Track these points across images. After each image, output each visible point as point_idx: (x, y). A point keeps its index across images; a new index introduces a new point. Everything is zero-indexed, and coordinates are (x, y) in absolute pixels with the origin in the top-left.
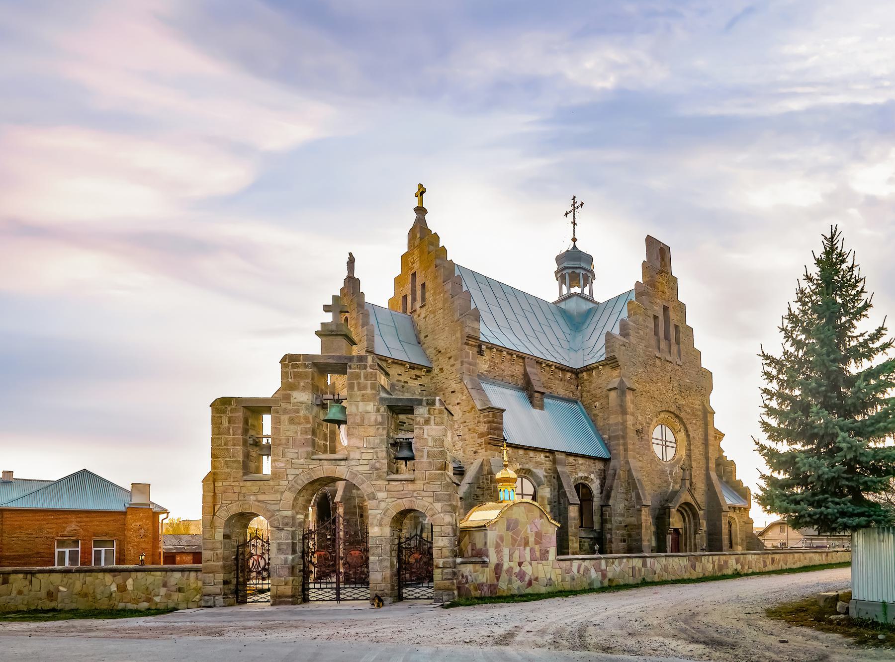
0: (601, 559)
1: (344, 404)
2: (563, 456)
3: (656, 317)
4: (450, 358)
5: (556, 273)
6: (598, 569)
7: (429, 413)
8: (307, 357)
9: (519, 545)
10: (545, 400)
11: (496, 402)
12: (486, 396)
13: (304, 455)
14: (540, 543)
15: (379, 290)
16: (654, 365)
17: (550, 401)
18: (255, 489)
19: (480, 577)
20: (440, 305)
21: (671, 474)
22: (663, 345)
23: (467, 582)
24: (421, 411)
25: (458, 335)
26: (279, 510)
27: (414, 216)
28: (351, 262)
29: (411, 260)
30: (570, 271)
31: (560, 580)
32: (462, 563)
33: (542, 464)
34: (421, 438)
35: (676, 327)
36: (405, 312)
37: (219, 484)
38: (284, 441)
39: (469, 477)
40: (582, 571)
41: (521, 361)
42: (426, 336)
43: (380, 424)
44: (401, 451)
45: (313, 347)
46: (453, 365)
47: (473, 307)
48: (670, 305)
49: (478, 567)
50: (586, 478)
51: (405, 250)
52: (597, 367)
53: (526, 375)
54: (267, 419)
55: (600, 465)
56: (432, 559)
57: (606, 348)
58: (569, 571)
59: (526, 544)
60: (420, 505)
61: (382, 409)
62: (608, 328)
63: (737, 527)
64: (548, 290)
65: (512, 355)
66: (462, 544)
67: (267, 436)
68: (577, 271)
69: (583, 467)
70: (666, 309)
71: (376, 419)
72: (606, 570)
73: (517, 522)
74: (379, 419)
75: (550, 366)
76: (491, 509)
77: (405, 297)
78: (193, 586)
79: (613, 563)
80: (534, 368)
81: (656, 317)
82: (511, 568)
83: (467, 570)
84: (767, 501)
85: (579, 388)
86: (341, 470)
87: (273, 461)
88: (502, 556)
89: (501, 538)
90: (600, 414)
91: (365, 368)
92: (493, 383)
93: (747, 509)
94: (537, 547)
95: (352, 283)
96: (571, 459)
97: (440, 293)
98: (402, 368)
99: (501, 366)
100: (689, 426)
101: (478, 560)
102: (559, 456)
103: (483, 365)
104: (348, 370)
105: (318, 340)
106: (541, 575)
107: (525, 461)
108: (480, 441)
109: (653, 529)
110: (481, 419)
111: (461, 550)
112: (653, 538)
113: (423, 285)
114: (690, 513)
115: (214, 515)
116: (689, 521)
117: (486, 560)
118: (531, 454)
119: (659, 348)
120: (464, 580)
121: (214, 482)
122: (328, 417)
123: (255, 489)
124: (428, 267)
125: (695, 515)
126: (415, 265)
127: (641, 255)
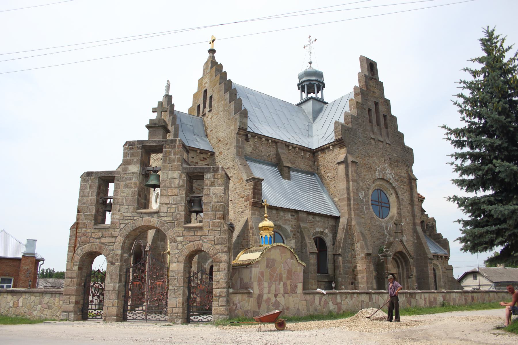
0: (336, 294)
1: (160, 173)
2: (304, 215)
3: (370, 110)
4: (226, 144)
5: (298, 85)
6: (335, 303)
7: (214, 178)
8: (140, 142)
9: (275, 280)
10: (291, 173)
11: (257, 175)
12: (250, 170)
13: (132, 209)
14: (291, 279)
15: (183, 104)
16: (370, 144)
17: (295, 173)
18: (100, 234)
19: (247, 305)
20: (221, 109)
21: (386, 229)
22: (376, 129)
23: (236, 309)
24: (208, 176)
25: (233, 128)
26: (113, 250)
27: (208, 55)
28: (168, 86)
29: (204, 81)
30: (308, 83)
31: (306, 310)
32: (234, 293)
33: (289, 221)
34: (208, 196)
35: (385, 116)
36: (198, 115)
37: (79, 231)
38: (120, 200)
39: (236, 233)
40: (322, 303)
41: (274, 144)
42: (211, 131)
43: (182, 186)
44: (194, 205)
45: (144, 135)
46: (229, 149)
47: (243, 109)
48: (380, 101)
49: (245, 297)
50: (322, 233)
51: (201, 75)
52: (329, 148)
53: (278, 154)
54: (111, 186)
55: (332, 222)
56: (212, 289)
57: (335, 132)
58: (313, 302)
59: (281, 279)
60: (206, 246)
61: (184, 176)
62: (336, 119)
63: (440, 272)
64: (294, 96)
65: (268, 140)
66: (233, 278)
67: (110, 198)
68: (313, 83)
69: (319, 224)
70: (376, 104)
71: (179, 183)
72: (341, 303)
73: (274, 261)
74: (181, 183)
75: (295, 148)
76: (256, 251)
77: (199, 106)
78: (57, 304)
79: (346, 298)
80: (283, 149)
81: (370, 110)
82: (269, 299)
83: (237, 298)
84: (474, 243)
85: (316, 163)
86: (154, 221)
87: (113, 214)
88: (262, 289)
89: (262, 274)
90: (332, 183)
91: (175, 147)
92: (255, 161)
93: (447, 258)
94: (288, 282)
95: (169, 98)
96: (311, 217)
97: (222, 100)
98: (195, 153)
99: (261, 149)
100: (398, 190)
101: (245, 291)
102: (302, 215)
103: (249, 148)
104: (164, 150)
105: (147, 131)
106: (291, 306)
107: (277, 219)
108: (246, 203)
109: (312, 322)
110: (247, 187)
111: (232, 283)
112: (374, 282)
113: (211, 97)
114: (402, 260)
115: (74, 253)
116: (402, 267)
117: (251, 291)
118: (282, 214)
119: (373, 131)
120: (235, 307)
121: (77, 229)
122: (148, 180)
123: (100, 234)
124: (215, 85)
125: (407, 262)
126: (207, 85)
127: (357, 68)
